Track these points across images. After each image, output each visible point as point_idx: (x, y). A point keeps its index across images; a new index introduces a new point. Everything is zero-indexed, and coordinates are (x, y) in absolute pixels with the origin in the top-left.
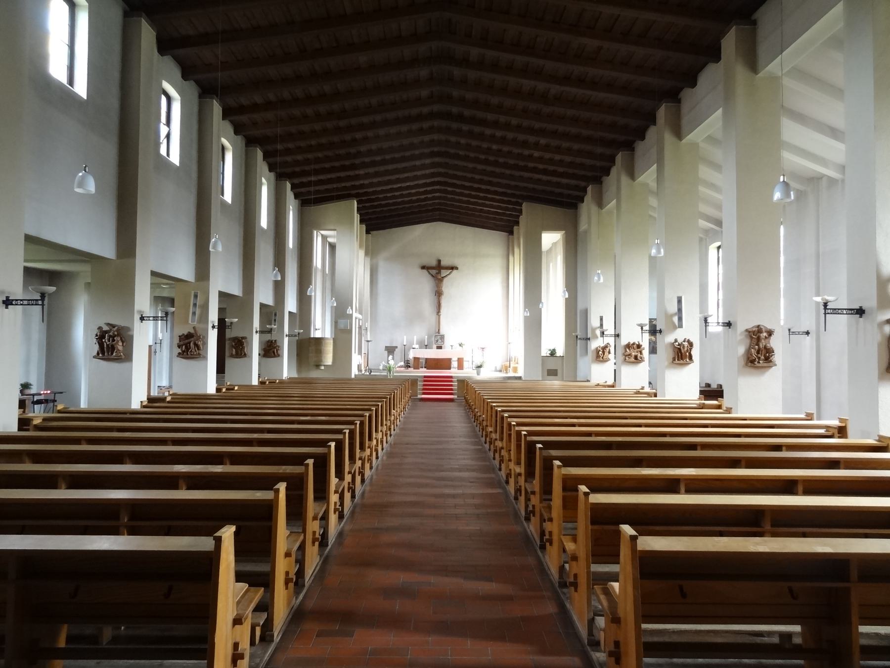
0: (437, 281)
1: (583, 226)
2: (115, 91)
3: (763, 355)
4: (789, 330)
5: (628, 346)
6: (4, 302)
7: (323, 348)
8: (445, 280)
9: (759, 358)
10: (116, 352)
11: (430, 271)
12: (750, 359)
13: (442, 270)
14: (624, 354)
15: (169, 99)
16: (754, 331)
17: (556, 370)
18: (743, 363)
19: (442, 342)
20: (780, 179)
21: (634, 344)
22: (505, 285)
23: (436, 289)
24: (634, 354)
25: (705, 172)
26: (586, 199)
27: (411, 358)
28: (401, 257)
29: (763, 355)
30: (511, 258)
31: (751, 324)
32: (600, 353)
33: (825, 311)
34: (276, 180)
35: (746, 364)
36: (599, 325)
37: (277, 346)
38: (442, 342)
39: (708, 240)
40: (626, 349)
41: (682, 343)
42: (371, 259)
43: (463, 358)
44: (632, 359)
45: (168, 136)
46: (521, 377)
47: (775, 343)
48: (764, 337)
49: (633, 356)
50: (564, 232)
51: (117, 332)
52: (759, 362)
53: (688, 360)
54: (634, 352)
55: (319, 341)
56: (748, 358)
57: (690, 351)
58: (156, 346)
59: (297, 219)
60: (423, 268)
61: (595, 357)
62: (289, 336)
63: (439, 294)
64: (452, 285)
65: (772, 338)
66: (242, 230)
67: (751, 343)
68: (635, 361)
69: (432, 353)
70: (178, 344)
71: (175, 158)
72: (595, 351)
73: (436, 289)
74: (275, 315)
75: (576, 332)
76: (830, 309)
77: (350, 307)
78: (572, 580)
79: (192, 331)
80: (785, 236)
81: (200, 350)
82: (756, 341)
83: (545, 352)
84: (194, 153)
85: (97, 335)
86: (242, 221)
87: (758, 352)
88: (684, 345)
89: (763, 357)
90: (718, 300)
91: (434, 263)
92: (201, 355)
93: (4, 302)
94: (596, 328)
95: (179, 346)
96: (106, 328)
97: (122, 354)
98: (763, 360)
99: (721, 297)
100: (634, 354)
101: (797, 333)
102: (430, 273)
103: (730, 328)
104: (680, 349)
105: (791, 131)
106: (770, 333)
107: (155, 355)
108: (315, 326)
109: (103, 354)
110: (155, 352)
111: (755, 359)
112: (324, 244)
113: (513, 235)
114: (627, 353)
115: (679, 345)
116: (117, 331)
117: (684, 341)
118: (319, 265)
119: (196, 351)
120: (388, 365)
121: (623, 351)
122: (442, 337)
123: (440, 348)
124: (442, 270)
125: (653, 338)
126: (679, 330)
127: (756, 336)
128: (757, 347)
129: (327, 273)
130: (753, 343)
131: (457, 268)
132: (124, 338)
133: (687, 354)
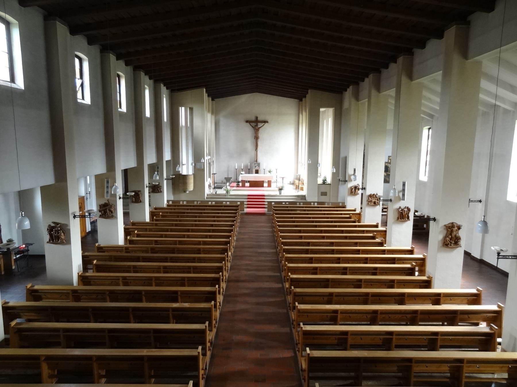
0: (255, 130)
1: (346, 105)
2: (43, 74)
3: (454, 240)
5: (370, 196)
7: (187, 181)
8: (260, 130)
9: (451, 243)
10: (60, 240)
11: (251, 124)
12: (445, 243)
13: (258, 123)
14: (367, 201)
15: (81, 60)
16: (450, 227)
17: (326, 192)
18: (441, 245)
19: (259, 167)
21: (374, 195)
22: (297, 132)
23: (255, 135)
24: (373, 200)
25: (425, 93)
26: (348, 90)
28: (234, 115)
29: (454, 240)
30: (301, 116)
31: (448, 221)
32: (353, 190)
33: (498, 257)
34: (154, 83)
35: (443, 246)
36: (353, 173)
37: (160, 186)
38: (259, 167)
39: (423, 123)
40: (369, 198)
41: (403, 209)
42: (215, 117)
43: (271, 181)
44: (373, 204)
45: (82, 85)
46: (305, 196)
47: (461, 233)
48: (455, 230)
49: (373, 202)
50: (334, 108)
51: (60, 228)
52: (451, 245)
53: (406, 219)
54: (374, 199)
55: (185, 177)
56: (444, 242)
57: (408, 214)
58: (87, 195)
59: (168, 101)
60: (247, 122)
61: (350, 193)
62: (166, 179)
63: (256, 138)
64: (264, 132)
65: (460, 230)
66: (134, 126)
67: (447, 233)
68: (374, 205)
69: (253, 177)
70: (99, 210)
71: (88, 101)
72: (350, 189)
73: (255, 135)
74: (158, 168)
75: (339, 177)
76: (501, 256)
77: (203, 158)
79: (107, 202)
81: (113, 213)
82: (450, 232)
83: (320, 181)
84: (100, 91)
85: (48, 230)
86: (134, 120)
87: (451, 239)
88: (404, 211)
89: (454, 242)
90: (426, 161)
91: (253, 119)
92: (113, 216)
94: (351, 175)
95: (100, 211)
96: (53, 225)
97: (64, 241)
98: (453, 244)
99: (428, 159)
100: (373, 200)
101: (474, 201)
102: (251, 125)
104: (402, 213)
105: (484, 84)
106: (459, 228)
107: (87, 200)
108: (182, 162)
109: (53, 240)
110: (87, 199)
111: (449, 243)
112: (186, 109)
113: (302, 101)
114: (369, 200)
115: (402, 210)
116: (60, 227)
117: (405, 208)
118: (184, 124)
119: (110, 214)
120: (226, 189)
121: (367, 199)
122: (259, 165)
123: (257, 172)
124: (258, 123)
126: (402, 201)
127: (450, 229)
128: (450, 236)
129: (189, 126)
130: (448, 233)
131: (267, 122)
132: (65, 231)
133: (406, 216)
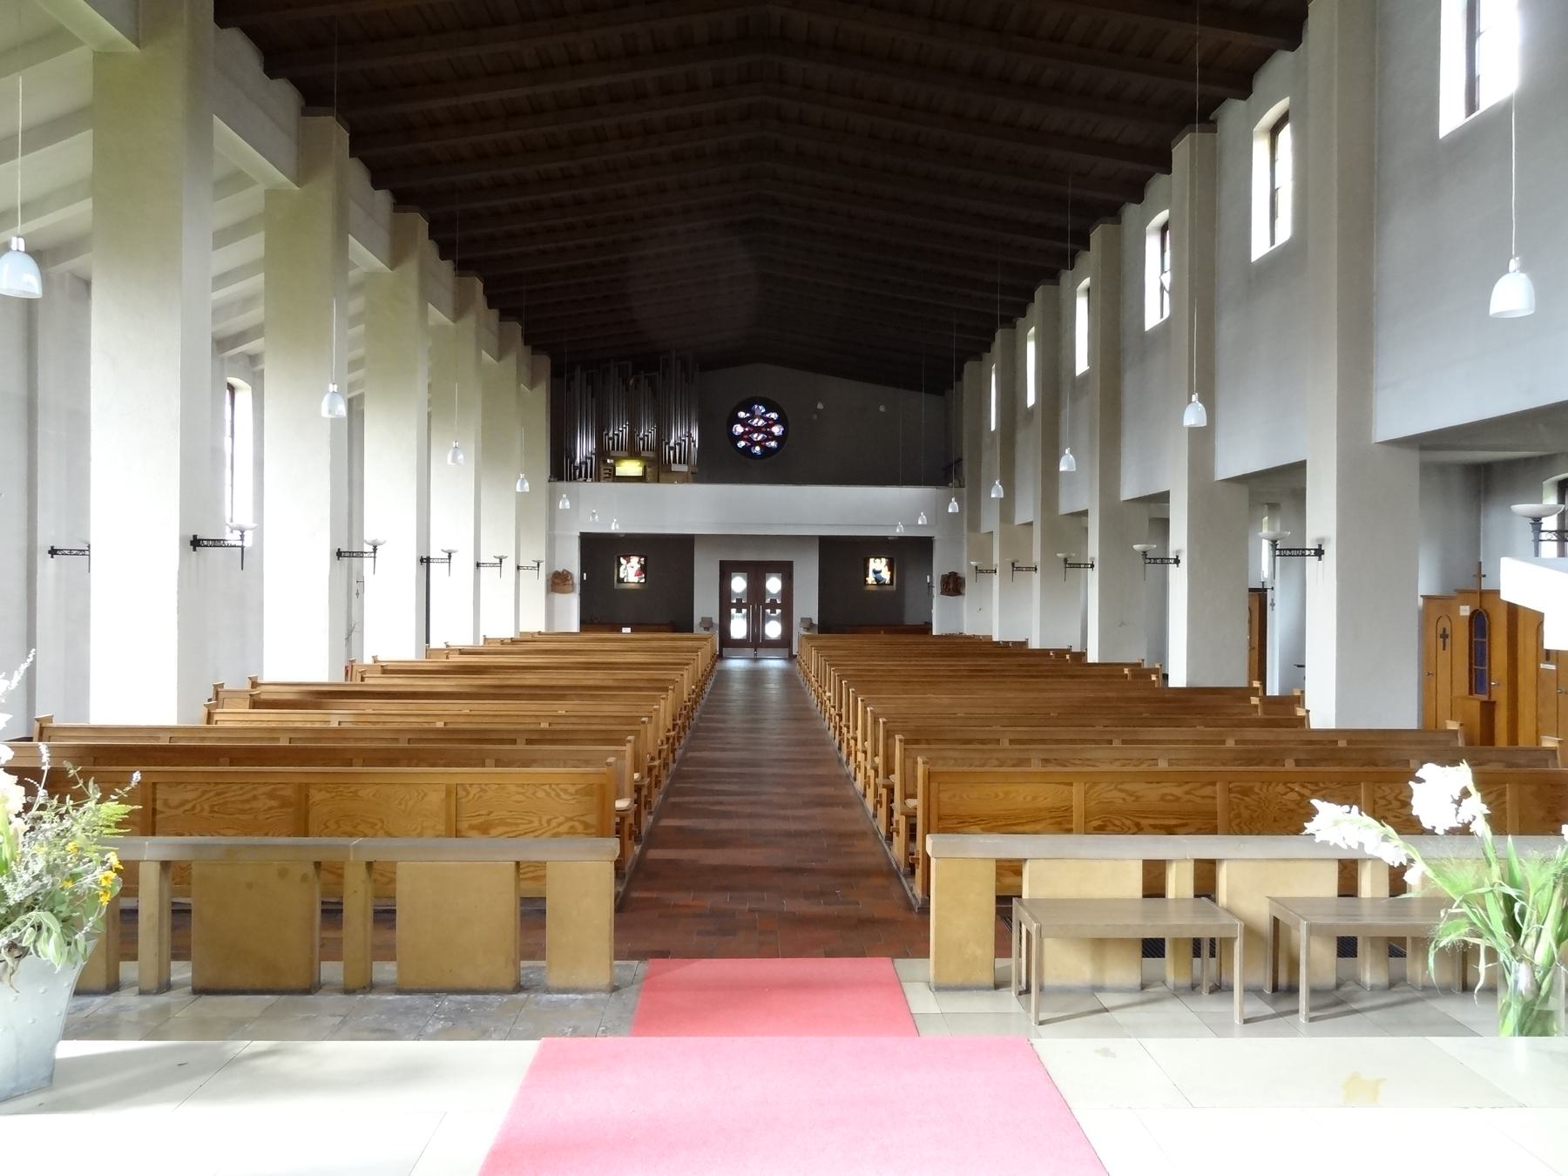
4: (1013, 564)
6: (50, 552)
20: (873, 591)
27: (636, 579)
78: (1383, 788)
80: (18, 120)
93: (50, 552)
101: (67, 552)
103: (1320, 559)
125: (44, 873)
